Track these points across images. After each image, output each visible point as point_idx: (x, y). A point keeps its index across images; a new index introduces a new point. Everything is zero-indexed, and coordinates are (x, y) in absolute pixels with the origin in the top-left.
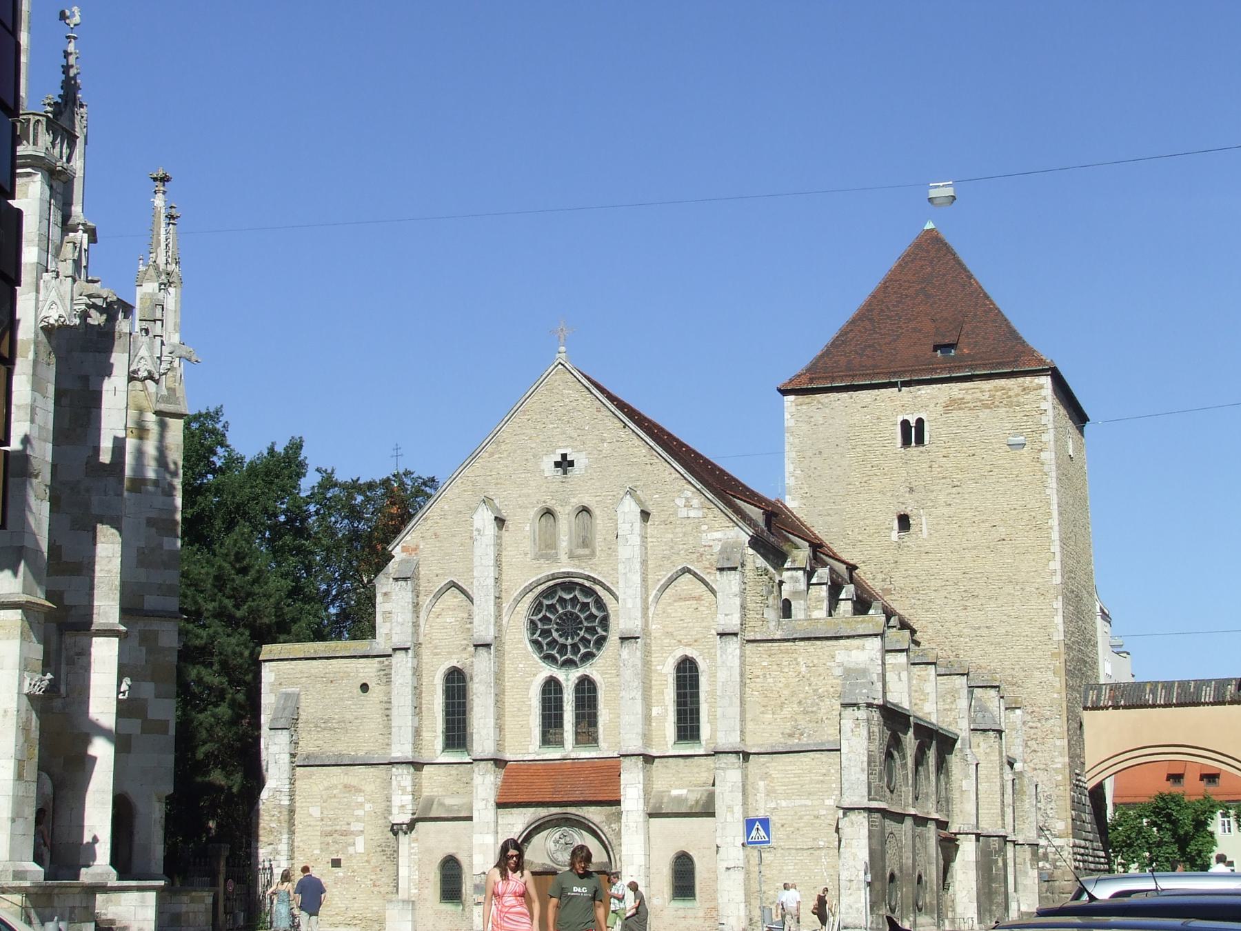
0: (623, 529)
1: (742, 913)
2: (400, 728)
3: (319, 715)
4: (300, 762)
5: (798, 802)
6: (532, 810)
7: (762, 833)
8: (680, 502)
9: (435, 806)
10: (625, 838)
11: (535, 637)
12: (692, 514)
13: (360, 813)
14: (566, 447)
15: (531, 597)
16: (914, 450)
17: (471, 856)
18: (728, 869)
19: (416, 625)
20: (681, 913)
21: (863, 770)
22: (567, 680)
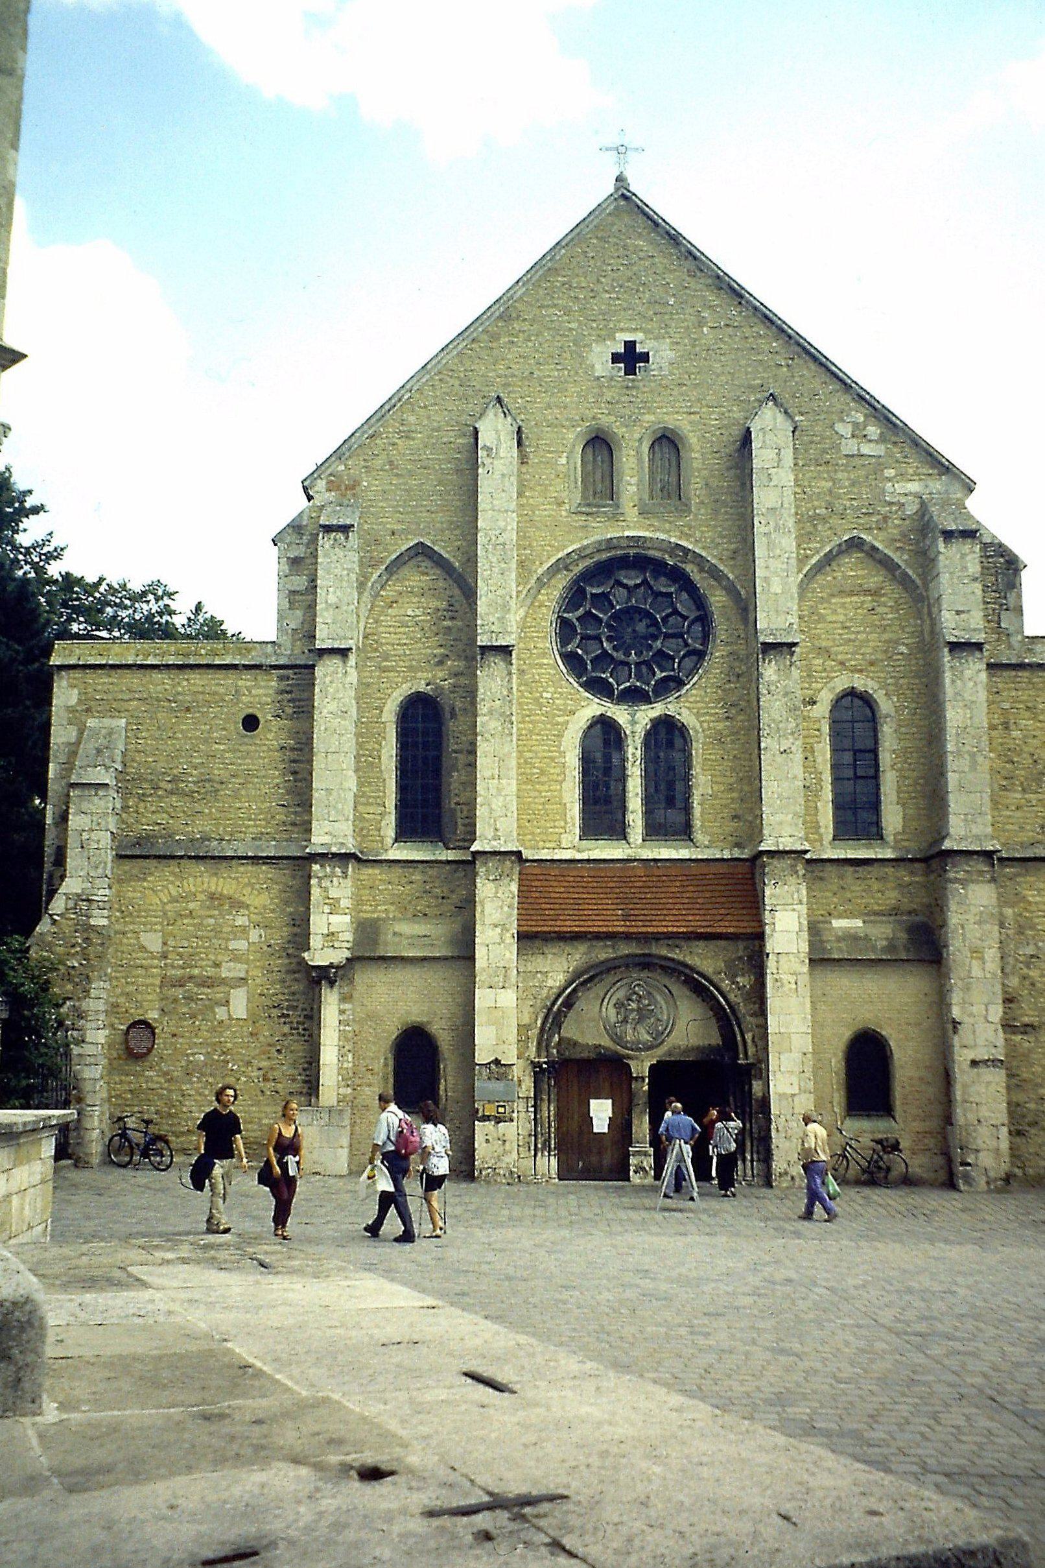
3: (161, 766)
4: (137, 852)
6: (582, 947)
8: (844, 429)
11: (569, 648)
13: (240, 945)
15: (562, 582)
18: (974, 1063)
22: (633, 723)
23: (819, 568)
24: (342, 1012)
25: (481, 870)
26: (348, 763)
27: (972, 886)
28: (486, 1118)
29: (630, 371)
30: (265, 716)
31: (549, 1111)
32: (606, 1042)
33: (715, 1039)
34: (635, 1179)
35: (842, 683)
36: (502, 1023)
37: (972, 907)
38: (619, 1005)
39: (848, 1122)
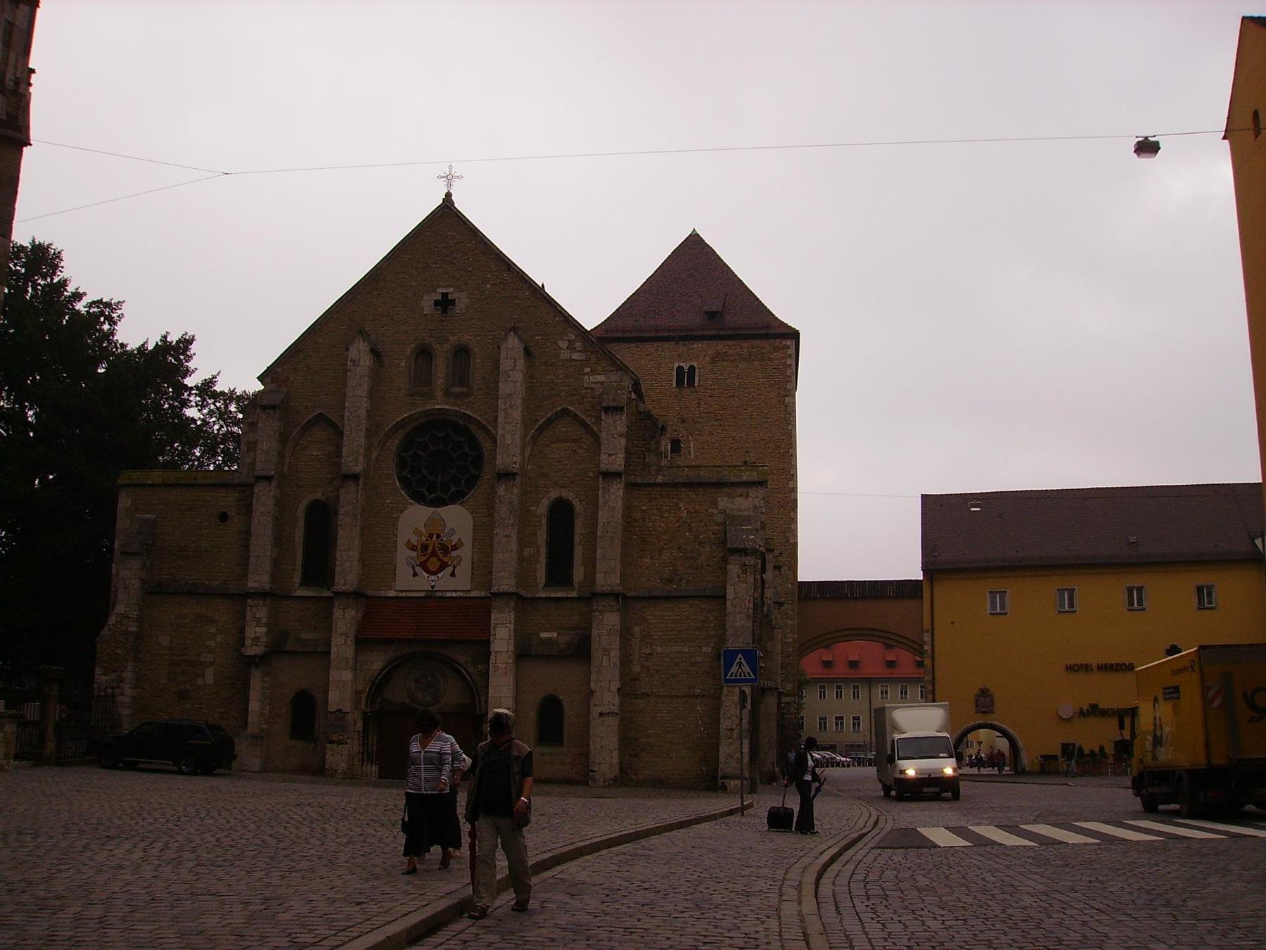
0: (506, 364)
1: (615, 760)
4: (155, 591)
7: (746, 668)
8: (563, 344)
10: (493, 680)
13: (212, 643)
14: (448, 286)
15: (399, 436)
17: (326, 692)
18: (601, 714)
19: (281, 455)
21: (748, 617)
23: (542, 429)
25: (336, 603)
28: (332, 742)
29: (445, 311)
35: (554, 494)
36: (343, 687)
37: (607, 623)
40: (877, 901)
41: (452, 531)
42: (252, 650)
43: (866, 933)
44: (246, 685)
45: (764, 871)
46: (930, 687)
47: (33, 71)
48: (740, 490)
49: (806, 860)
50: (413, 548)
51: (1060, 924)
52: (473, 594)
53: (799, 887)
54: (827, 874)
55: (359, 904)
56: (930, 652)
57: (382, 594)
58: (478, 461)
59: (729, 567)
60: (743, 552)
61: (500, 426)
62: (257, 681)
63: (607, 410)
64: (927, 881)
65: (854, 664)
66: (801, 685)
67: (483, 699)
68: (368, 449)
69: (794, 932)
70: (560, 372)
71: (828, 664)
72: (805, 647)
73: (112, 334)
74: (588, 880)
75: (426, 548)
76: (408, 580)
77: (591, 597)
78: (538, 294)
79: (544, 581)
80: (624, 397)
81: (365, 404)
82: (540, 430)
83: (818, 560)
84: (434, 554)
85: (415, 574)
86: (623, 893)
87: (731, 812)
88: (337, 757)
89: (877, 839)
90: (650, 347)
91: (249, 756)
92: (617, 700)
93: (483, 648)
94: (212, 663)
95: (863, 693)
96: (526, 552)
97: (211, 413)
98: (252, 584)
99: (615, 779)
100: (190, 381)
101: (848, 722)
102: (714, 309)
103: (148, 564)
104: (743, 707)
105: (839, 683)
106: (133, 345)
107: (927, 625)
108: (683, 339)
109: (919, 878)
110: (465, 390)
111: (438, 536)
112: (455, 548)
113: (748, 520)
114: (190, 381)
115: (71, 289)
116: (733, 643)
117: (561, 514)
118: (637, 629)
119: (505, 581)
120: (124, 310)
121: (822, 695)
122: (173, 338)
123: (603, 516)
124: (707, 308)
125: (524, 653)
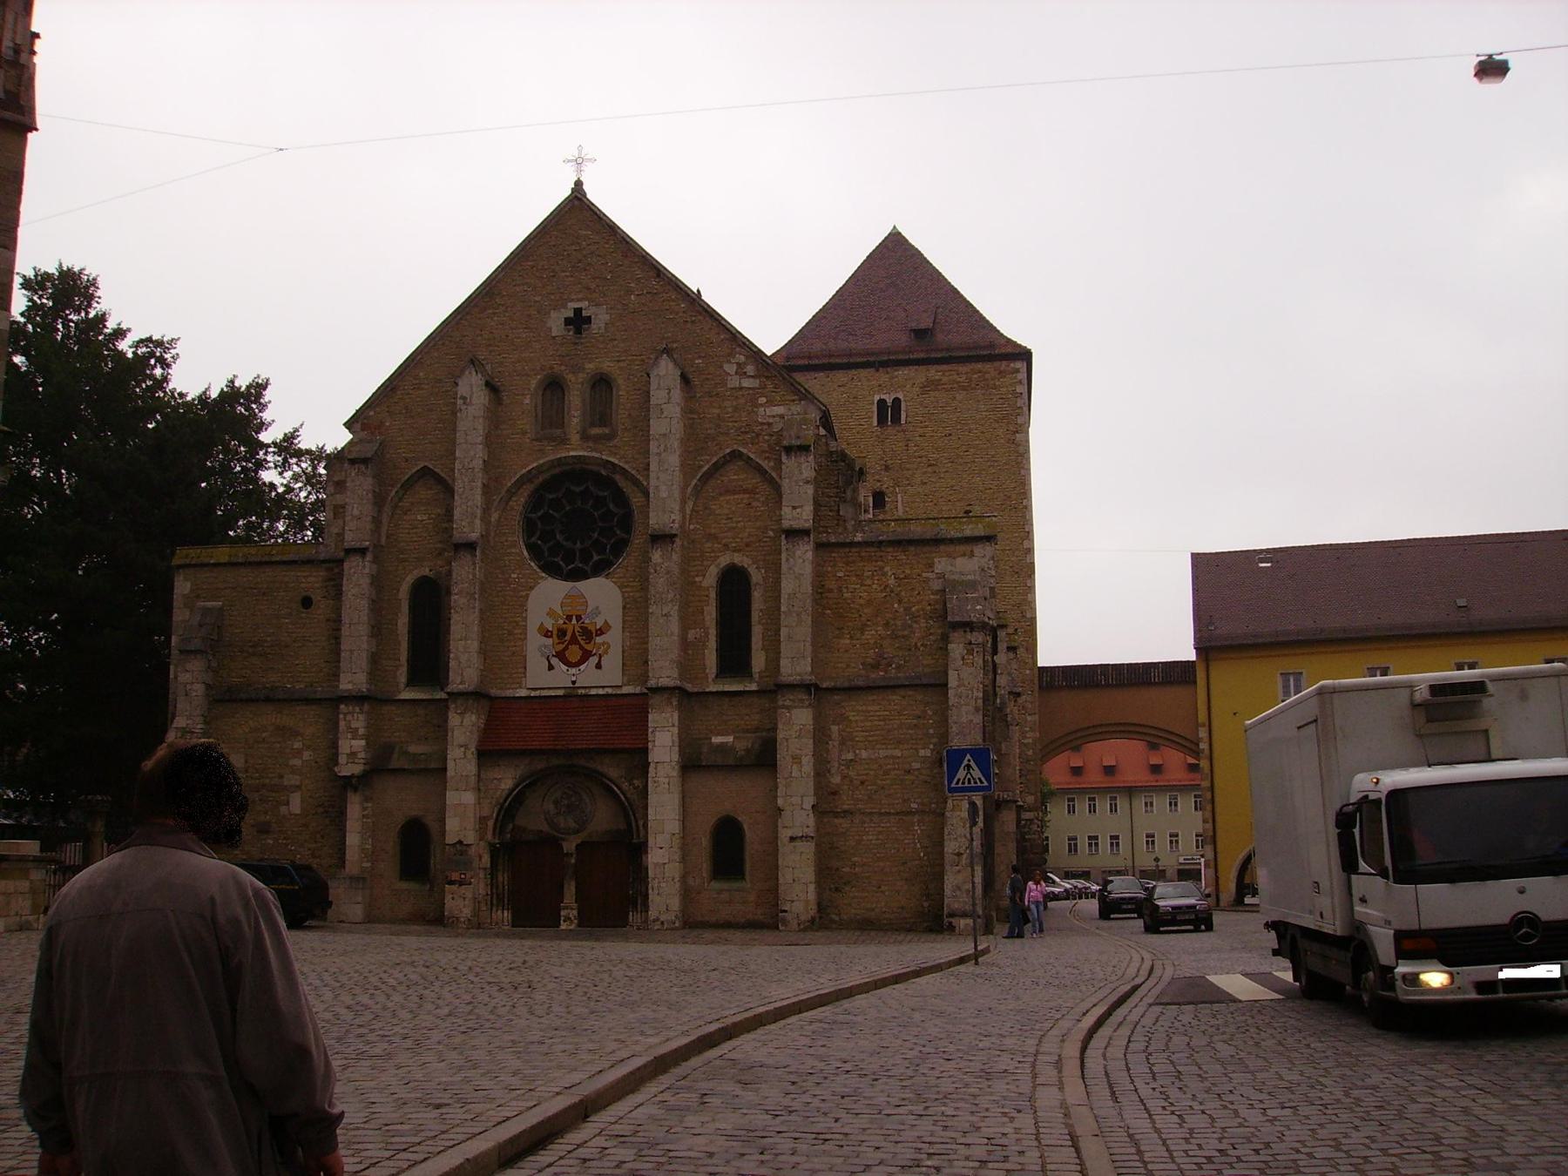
0: (657, 396)
1: (812, 896)
2: (351, 651)
4: (224, 698)
5: (882, 753)
7: (977, 773)
8: (730, 368)
9: (395, 756)
10: (652, 799)
12: (746, 383)
13: (297, 762)
16: (890, 430)
17: (443, 821)
18: (792, 839)
19: (377, 521)
20: (725, 896)
21: (977, 709)
24: (365, 809)
26: (363, 630)
27: (794, 711)
28: (451, 883)
29: (578, 331)
30: (316, 598)
31: (503, 877)
32: (545, 828)
33: (622, 826)
34: (563, 926)
35: (725, 560)
36: (463, 814)
37: (796, 722)
38: (556, 803)
39: (716, 885)
40: (1167, 1081)
41: (597, 611)
42: (347, 769)
43: (1157, 1131)
44: (343, 813)
45: (1009, 1042)
46: (1209, 795)
47: (37, 36)
48: (962, 548)
49: (1065, 1024)
50: (548, 634)
51: (1432, 1112)
52: (625, 690)
53: (1059, 1064)
54: (1093, 1043)
55: (438, 1106)
56: (1207, 752)
57: (509, 693)
58: (626, 522)
59: (950, 646)
60: (968, 626)
61: (652, 475)
62: (355, 808)
63: (789, 450)
64: (1232, 1051)
65: (1109, 770)
66: (1045, 797)
67: (641, 823)
68: (486, 510)
69: (1055, 1133)
70: (727, 403)
71: (1077, 771)
72: (1049, 749)
73: (165, 379)
74: (770, 1061)
75: (560, 634)
76: (543, 675)
77: (775, 690)
78: (693, 301)
79: (714, 670)
80: (809, 434)
81: (479, 453)
82: (704, 478)
83: (1063, 638)
84: (574, 640)
85: (551, 667)
86: (814, 1079)
87: (962, 961)
88: (459, 902)
89: (1155, 992)
90: (841, 377)
91: (347, 902)
92: (811, 821)
93: (638, 759)
94: (298, 787)
95: (1122, 803)
96: (691, 635)
97: (296, 478)
98: (346, 685)
99: (813, 920)
100: (265, 437)
101: (1104, 843)
102: (922, 326)
103: (214, 664)
104: (974, 823)
105: (1092, 793)
106: (192, 394)
107: (1202, 717)
108: (885, 364)
109: (1219, 1046)
110: (607, 431)
111: (579, 618)
112: (600, 632)
113: (973, 585)
114: (265, 437)
115: (111, 325)
116: (956, 743)
117: (734, 585)
118: (835, 728)
119: (664, 672)
120: (179, 348)
121: (1072, 810)
122: (242, 383)
123: (787, 586)
124: (914, 325)
125: (692, 764)
